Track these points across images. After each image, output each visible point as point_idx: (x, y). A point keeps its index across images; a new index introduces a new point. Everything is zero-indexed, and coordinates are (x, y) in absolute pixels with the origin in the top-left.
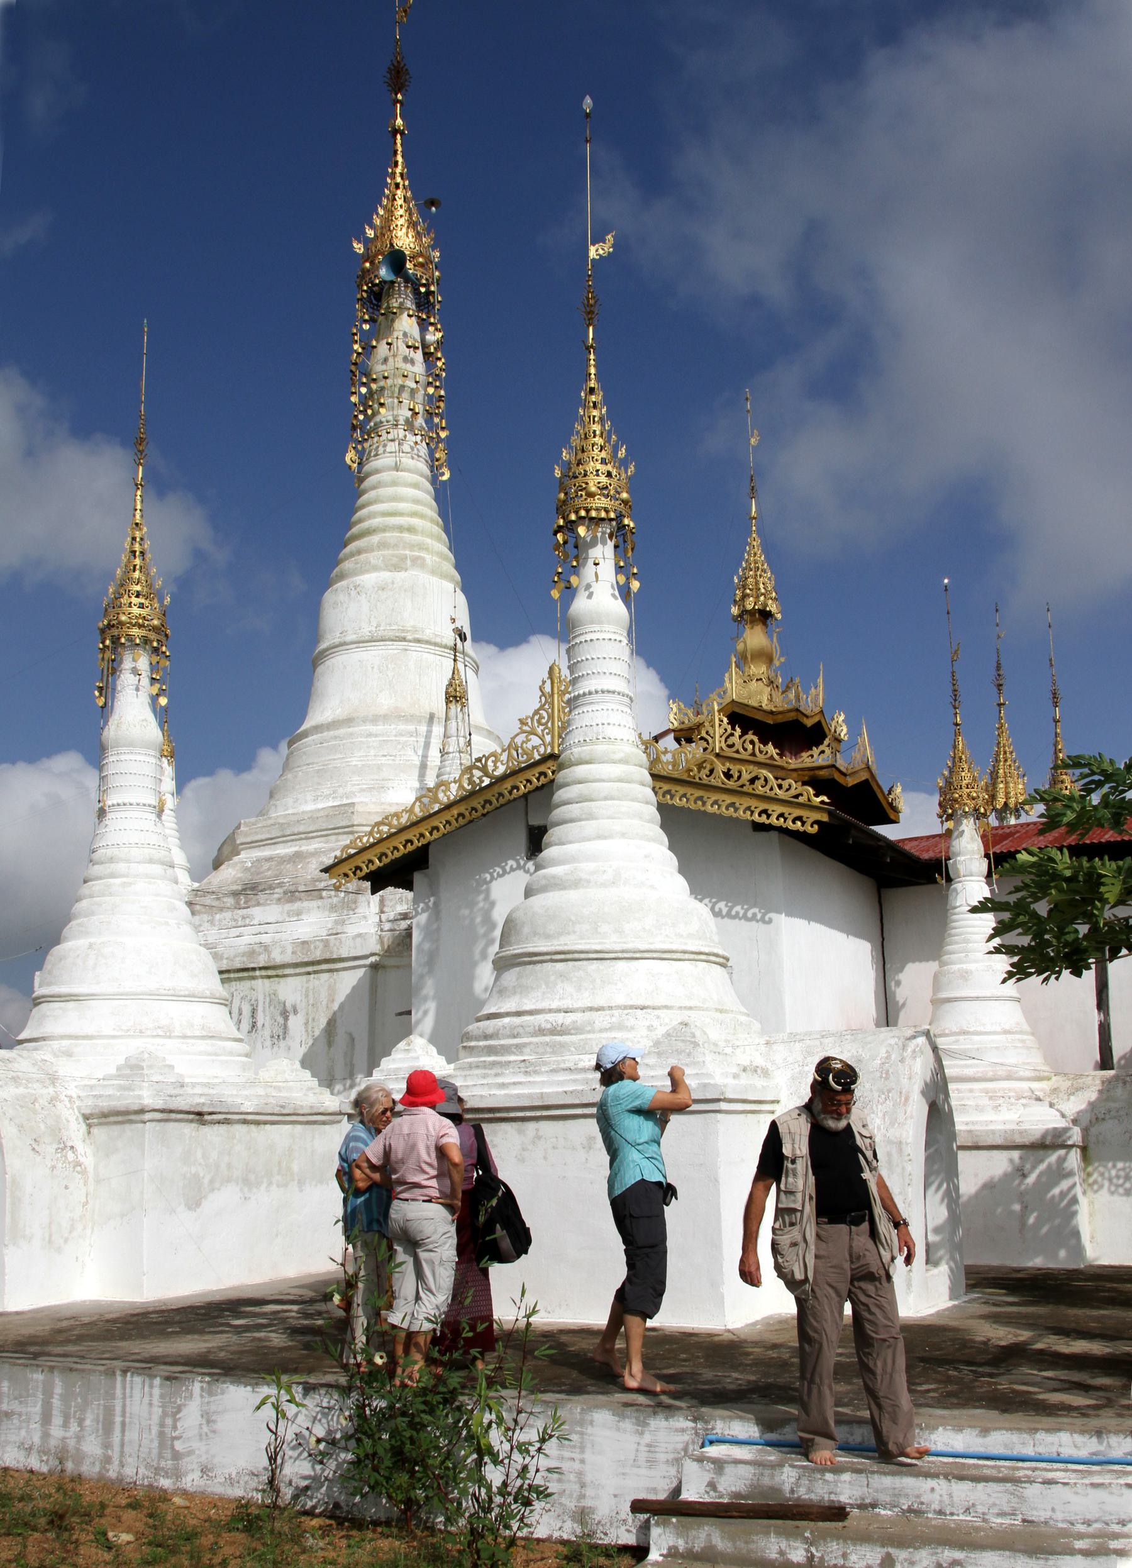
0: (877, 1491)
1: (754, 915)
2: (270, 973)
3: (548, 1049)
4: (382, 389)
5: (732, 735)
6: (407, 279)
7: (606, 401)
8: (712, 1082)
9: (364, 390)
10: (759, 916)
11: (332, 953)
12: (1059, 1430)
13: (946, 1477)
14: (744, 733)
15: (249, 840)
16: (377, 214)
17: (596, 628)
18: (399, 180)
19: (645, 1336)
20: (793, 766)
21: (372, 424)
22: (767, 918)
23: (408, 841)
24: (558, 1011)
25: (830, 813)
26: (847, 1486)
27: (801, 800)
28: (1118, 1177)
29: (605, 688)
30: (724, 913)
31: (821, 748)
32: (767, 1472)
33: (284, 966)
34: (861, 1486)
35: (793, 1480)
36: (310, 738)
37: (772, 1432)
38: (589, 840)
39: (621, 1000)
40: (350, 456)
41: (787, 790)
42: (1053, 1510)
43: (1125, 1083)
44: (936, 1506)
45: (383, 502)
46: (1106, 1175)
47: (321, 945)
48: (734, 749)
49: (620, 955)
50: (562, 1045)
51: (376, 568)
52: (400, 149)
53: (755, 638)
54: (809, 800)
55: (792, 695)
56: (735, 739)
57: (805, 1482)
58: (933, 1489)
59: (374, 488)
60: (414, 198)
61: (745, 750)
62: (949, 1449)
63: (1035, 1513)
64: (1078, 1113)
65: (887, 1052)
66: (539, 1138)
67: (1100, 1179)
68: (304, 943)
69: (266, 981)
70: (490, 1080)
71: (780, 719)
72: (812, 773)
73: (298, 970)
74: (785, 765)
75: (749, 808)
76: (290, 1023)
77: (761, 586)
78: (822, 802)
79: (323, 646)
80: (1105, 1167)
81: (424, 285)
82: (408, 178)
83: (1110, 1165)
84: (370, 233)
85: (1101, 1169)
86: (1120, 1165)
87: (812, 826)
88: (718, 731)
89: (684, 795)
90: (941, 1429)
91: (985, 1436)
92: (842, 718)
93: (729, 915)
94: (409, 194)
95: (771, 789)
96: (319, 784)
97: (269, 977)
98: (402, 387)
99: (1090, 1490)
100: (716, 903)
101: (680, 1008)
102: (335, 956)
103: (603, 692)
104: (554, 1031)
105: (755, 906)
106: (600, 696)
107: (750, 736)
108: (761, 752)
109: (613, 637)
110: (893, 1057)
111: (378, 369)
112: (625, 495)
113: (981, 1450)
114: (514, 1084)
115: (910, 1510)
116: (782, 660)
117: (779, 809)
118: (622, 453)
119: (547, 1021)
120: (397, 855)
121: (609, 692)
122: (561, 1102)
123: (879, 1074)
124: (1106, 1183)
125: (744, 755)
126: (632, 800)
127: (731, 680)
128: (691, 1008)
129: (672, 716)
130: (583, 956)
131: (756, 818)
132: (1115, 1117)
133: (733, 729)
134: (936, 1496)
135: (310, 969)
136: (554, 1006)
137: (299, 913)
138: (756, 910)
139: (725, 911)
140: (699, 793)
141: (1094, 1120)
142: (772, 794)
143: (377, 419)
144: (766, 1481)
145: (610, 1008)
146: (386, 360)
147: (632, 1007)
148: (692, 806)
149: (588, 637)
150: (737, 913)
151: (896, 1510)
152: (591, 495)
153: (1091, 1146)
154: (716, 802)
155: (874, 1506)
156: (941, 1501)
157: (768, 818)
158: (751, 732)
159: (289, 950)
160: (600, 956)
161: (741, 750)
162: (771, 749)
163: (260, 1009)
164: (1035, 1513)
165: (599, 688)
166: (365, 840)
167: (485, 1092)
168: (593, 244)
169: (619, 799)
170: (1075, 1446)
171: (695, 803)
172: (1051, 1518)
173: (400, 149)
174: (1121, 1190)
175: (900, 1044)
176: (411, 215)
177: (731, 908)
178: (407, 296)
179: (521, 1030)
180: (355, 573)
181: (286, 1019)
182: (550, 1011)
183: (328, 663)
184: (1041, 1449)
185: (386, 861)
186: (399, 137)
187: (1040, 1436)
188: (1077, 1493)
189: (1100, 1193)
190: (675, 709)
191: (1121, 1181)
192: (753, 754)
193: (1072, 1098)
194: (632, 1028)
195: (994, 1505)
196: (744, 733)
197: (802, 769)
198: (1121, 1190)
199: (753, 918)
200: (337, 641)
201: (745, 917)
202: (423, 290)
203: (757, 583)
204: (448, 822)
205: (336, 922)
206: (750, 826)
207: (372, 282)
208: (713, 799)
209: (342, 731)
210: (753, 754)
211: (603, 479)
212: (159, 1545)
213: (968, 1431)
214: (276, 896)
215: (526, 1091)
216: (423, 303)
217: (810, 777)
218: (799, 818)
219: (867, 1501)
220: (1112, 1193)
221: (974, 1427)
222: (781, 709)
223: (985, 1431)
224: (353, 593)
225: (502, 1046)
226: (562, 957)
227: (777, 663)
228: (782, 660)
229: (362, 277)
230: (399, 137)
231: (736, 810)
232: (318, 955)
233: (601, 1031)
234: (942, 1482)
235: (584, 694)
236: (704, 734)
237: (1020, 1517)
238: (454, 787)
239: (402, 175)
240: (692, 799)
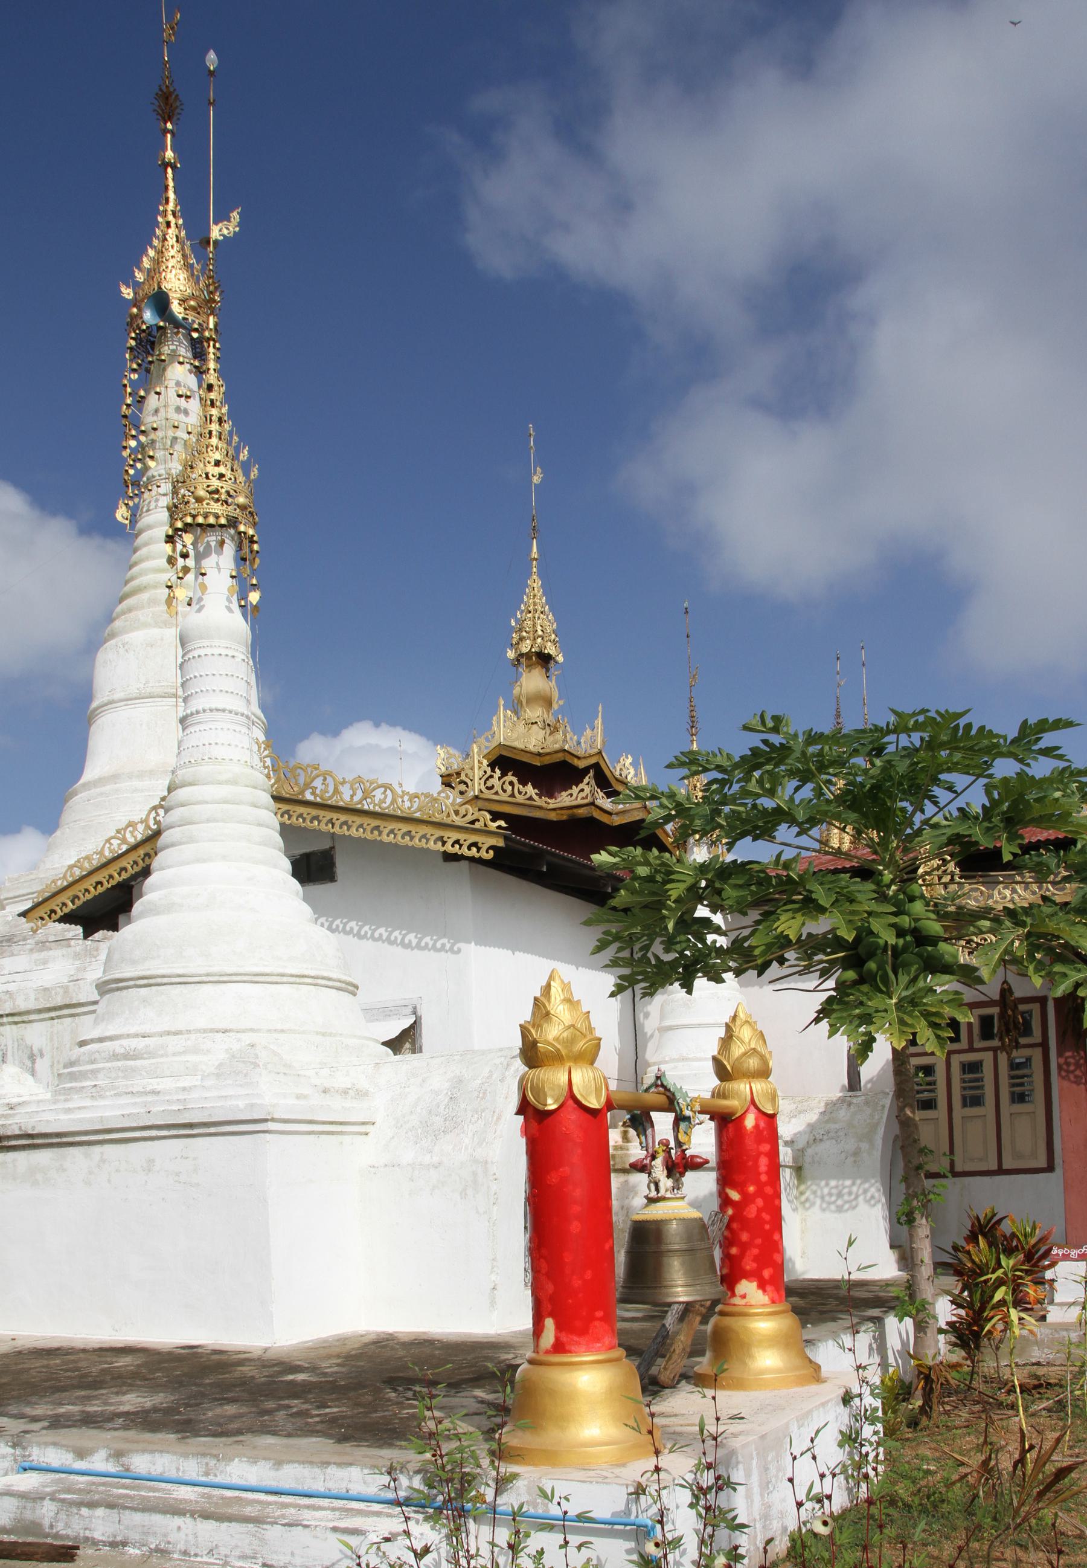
0: (127, 1528)
1: (443, 945)
2: (16, 1019)
3: (120, 1074)
4: (153, 442)
5: (491, 777)
6: (176, 324)
7: (228, 398)
8: (259, 1102)
9: (133, 443)
10: (448, 946)
11: (71, 998)
12: (351, 1464)
13: (192, 1516)
14: (504, 774)
15: (11, 895)
16: (147, 255)
17: (205, 643)
18: (170, 218)
20: (551, 806)
21: (145, 479)
22: (455, 949)
23: (98, 883)
24: (136, 1036)
25: (506, 838)
26: (100, 1522)
27: (477, 825)
28: (830, 1195)
29: (213, 707)
30: (414, 944)
31: (581, 786)
32: (29, 1505)
33: (28, 1012)
34: (113, 1522)
35: (52, 1514)
36: (80, 796)
38: (188, 864)
39: (201, 1023)
40: (122, 514)
41: (464, 816)
42: (293, 1554)
43: (849, 1105)
44: (181, 1546)
45: (154, 558)
46: (819, 1193)
47: (61, 991)
48: (493, 791)
49: (205, 979)
50: (134, 1070)
51: (146, 625)
52: (171, 184)
53: (533, 681)
54: (486, 825)
55: (559, 736)
56: (495, 781)
57: (63, 1516)
58: (179, 1528)
59: (146, 544)
60: (189, 237)
61: (504, 791)
64: (795, 1134)
65: (490, 1071)
66: (103, 1161)
67: (812, 1197)
68: (46, 989)
69: (14, 1027)
70: (60, 1106)
71: (547, 760)
72: (570, 812)
73: (42, 1016)
74: (544, 805)
75: (424, 836)
76: (37, 1066)
77: (539, 628)
78: (499, 827)
79: (94, 705)
80: (818, 1185)
81: (196, 330)
82: (182, 217)
83: (823, 1183)
84: (140, 277)
85: (814, 1187)
86: (833, 1183)
87: (487, 852)
88: (478, 773)
89: (361, 826)
91: (277, 1470)
92: (630, 760)
93: (418, 947)
94: (183, 233)
95: (448, 815)
96: (84, 839)
97: (16, 1023)
98: (175, 439)
100: (375, 930)
101: (269, 1031)
102: (74, 1002)
103: (211, 710)
104: (126, 1056)
105: (445, 936)
106: (208, 715)
107: (510, 777)
108: (520, 793)
109: (224, 652)
110: (494, 1076)
111: (149, 420)
112: (241, 500)
113: (273, 1484)
114: (79, 1108)
115: (157, 1550)
116: (561, 702)
117: (455, 836)
118: (244, 455)
119: (121, 1046)
120: (89, 897)
121: (218, 710)
122: (119, 1126)
123: (476, 1094)
124: (818, 1201)
125: (504, 797)
126: (239, 822)
127: (498, 722)
128: (282, 1031)
129: (439, 763)
130: (165, 980)
131: (448, 848)
132: (832, 1138)
133: (493, 771)
134: (182, 1535)
135: (53, 1014)
136: (132, 1031)
137: (45, 962)
138: (445, 941)
139: (414, 942)
140: (375, 823)
141: (811, 1141)
142: (448, 821)
143: (149, 473)
144: (28, 1515)
145: (189, 1032)
146: (157, 411)
147: (212, 1031)
148: (369, 836)
149: (196, 653)
150: (427, 944)
151: (144, 1548)
152: (199, 500)
153: (806, 1166)
154: (392, 831)
155: (124, 1544)
156: (186, 1541)
157: (411, 840)
158: (510, 774)
159: (32, 997)
160: (183, 981)
161: (500, 791)
162: (530, 790)
163: (9, 1054)
165: (207, 707)
166: (59, 883)
167: (50, 1117)
168: (216, 223)
169: (223, 821)
170: (365, 1483)
171: (311, 822)
172: (290, 1563)
173: (171, 184)
174: (833, 1207)
175: (505, 1064)
176: (184, 256)
177: (421, 940)
178: (180, 342)
179: (97, 1056)
180: (124, 631)
181: (34, 1062)
182: (128, 1036)
183: (99, 722)
185: (78, 903)
186: (169, 170)
187: (332, 1470)
188: (316, 1537)
189: (811, 1210)
190: (442, 755)
191: (833, 1198)
192: (513, 795)
193: (793, 1120)
194: (208, 1051)
196: (504, 774)
197: (561, 809)
198: (833, 1207)
199: (443, 948)
200: (105, 699)
201: (434, 948)
202: (195, 335)
203: (534, 625)
204: (135, 863)
205: (78, 970)
206: (440, 859)
207: (139, 328)
208: (390, 828)
209: (107, 788)
210: (513, 795)
211: (215, 483)
213: (262, 1463)
214: (28, 947)
215: (88, 1116)
216: (198, 350)
217: (569, 816)
218: (475, 844)
219: (119, 1539)
220: (824, 1210)
221: (269, 1459)
222: (548, 751)
223: (279, 1464)
224: (122, 651)
225: (80, 1072)
226: (145, 982)
227: (555, 706)
228: (561, 702)
229: (130, 324)
230: (169, 170)
231: (412, 838)
232: (59, 1001)
233: (174, 1055)
234: (188, 1520)
235: (192, 714)
236: (463, 777)
238: (141, 827)
239: (174, 214)
240: (369, 829)
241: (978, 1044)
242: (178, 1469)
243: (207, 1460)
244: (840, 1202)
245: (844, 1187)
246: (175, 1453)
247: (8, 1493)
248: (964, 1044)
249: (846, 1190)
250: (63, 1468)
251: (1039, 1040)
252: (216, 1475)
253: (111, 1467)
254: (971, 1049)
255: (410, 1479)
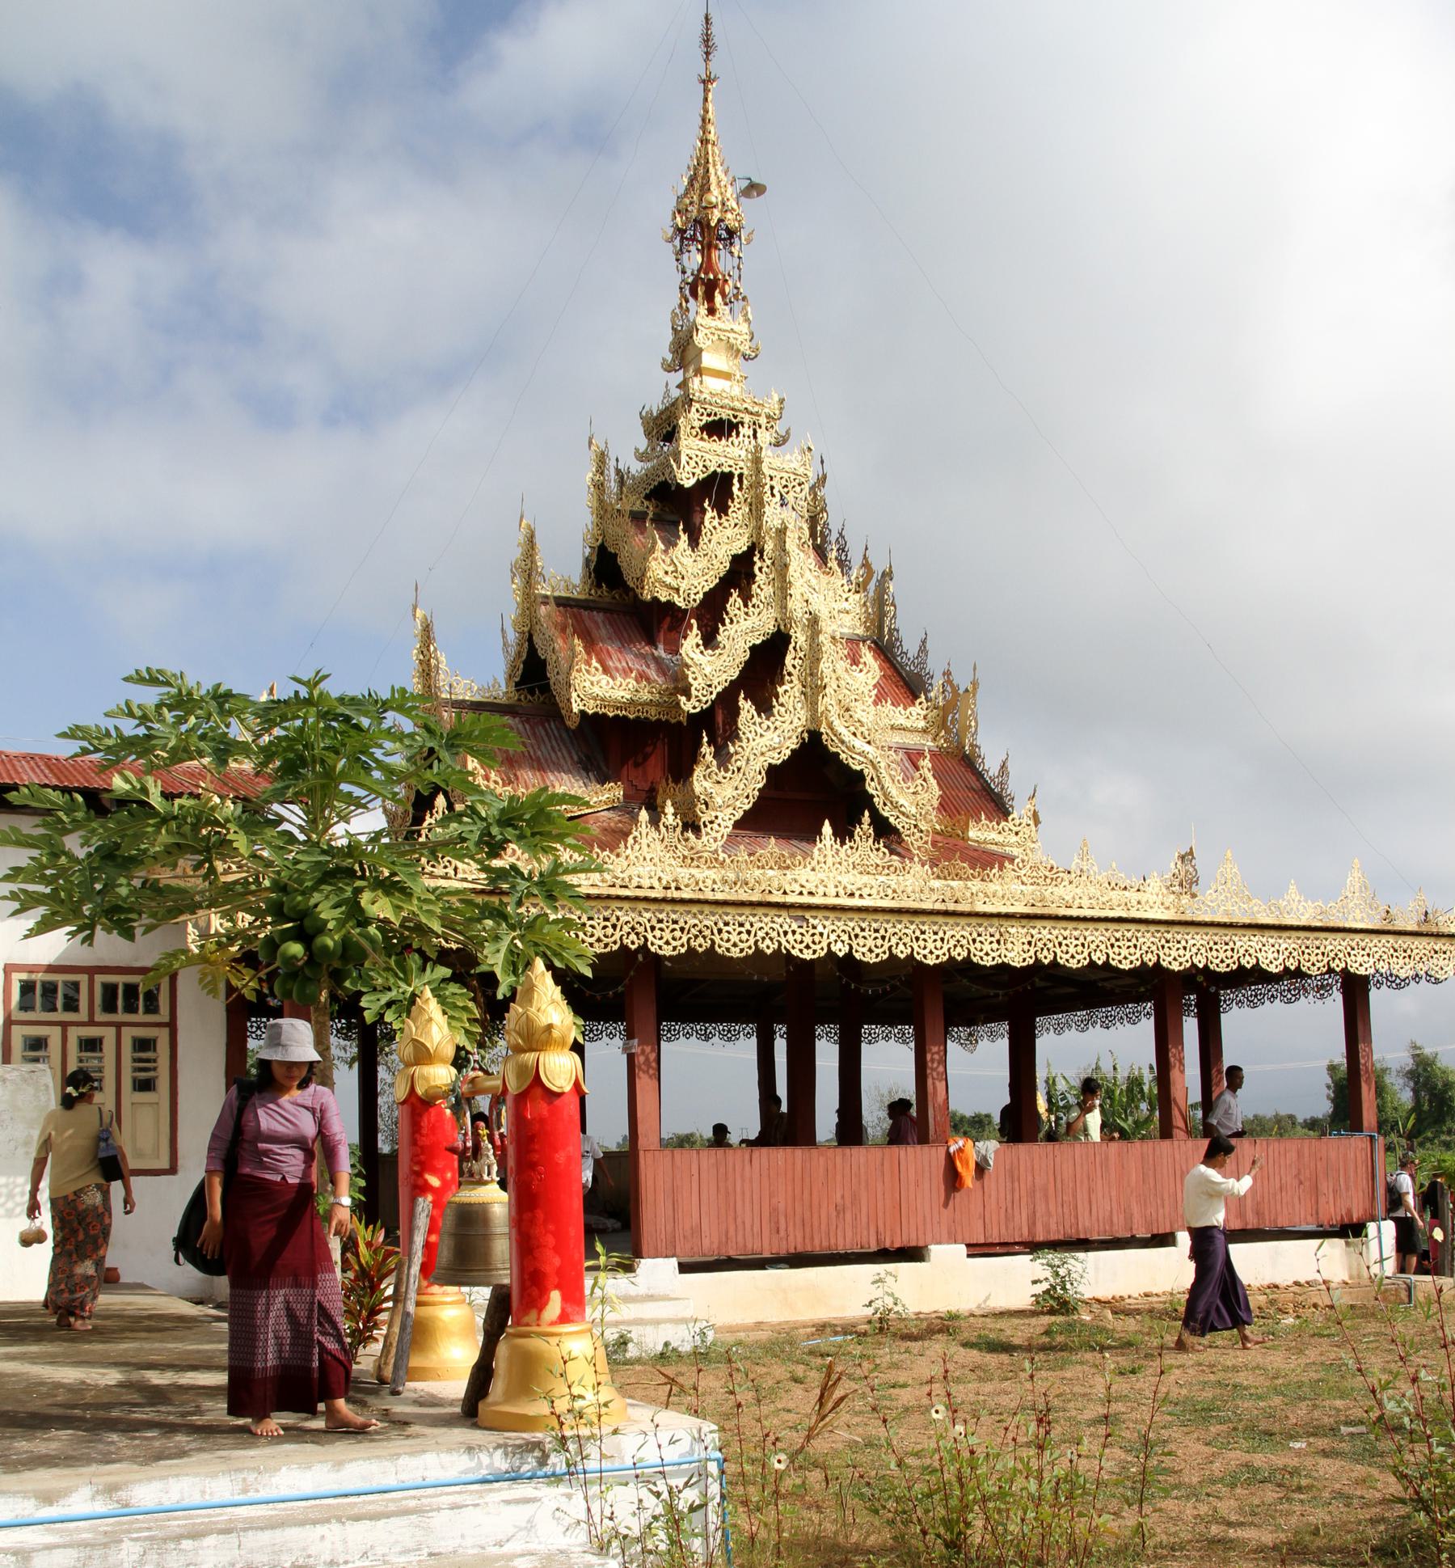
0: (251, 1551)
12: (424, 1452)
19: (730, 475)
32: (97, 1553)
35: (135, 1557)
37: (51, 1504)
58: (323, 1537)
62: (295, 1493)
63: (443, 1543)
90: (284, 1469)
99: (504, 1508)
113: (336, 1488)
164: (443, 1543)
184: (403, 1476)
187: (404, 1461)
195: (397, 1542)
212: (962, 1486)
213: (317, 1467)
223: (339, 1465)
234: (335, 1526)
237: (425, 1551)
241: (100, 1017)
242: (203, 1492)
243: (245, 1474)
244: (10, 1205)
245: (16, 1186)
246: (197, 1475)
247: (5, 1551)
248: (83, 1015)
249: (18, 1190)
250: (20, 1520)
251: (167, 1019)
252: (257, 1491)
253: (100, 1506)
254: (91, 1022)
255: (491, 1456)
